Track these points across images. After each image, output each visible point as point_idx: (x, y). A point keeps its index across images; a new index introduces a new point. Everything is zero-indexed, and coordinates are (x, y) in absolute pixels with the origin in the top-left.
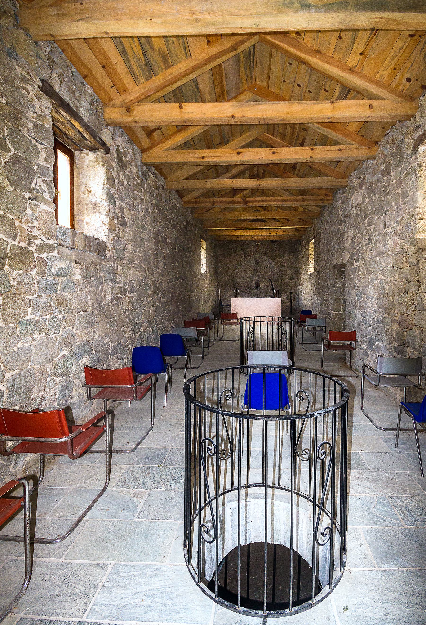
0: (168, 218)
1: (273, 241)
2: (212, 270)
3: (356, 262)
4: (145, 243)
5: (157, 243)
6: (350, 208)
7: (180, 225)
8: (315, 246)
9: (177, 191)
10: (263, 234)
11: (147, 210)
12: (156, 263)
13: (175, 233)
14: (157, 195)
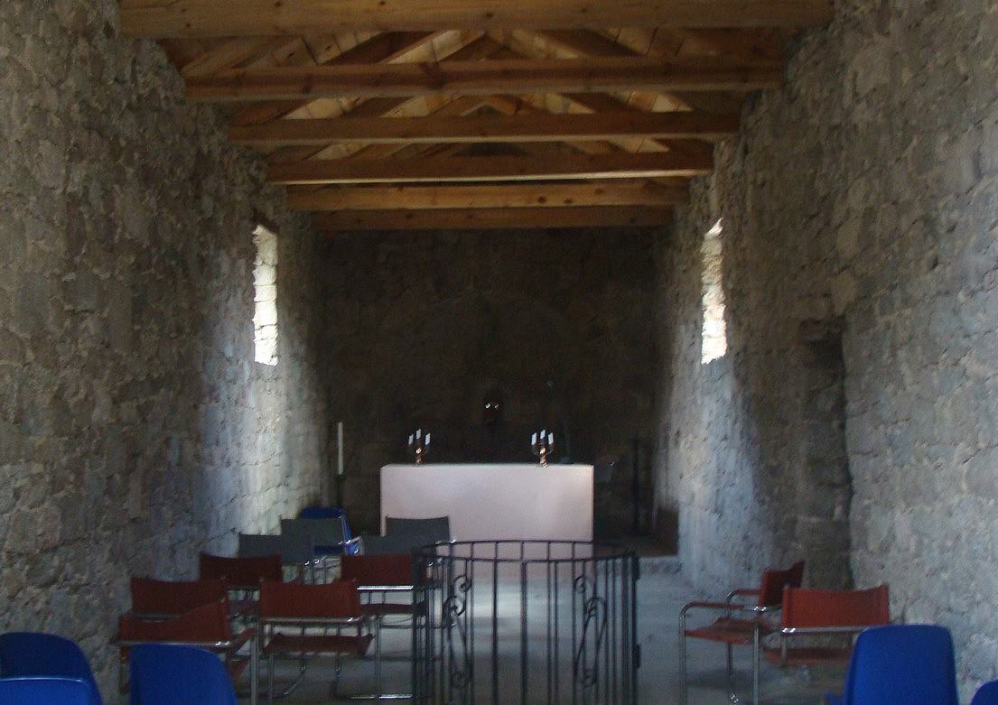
0: (123, 143)
1: (554, 232)
2: (302, 350)
3: (883, 313)
4: (30, 241)
5: (75, 240)
6: (847, 101)
7: (172, 172)
8: (725, 248)
9: (163, 42)
10: (516, 202)
11: (41, 112)
12: (67, 323)
13: (152, 201)
14: (83, 60)
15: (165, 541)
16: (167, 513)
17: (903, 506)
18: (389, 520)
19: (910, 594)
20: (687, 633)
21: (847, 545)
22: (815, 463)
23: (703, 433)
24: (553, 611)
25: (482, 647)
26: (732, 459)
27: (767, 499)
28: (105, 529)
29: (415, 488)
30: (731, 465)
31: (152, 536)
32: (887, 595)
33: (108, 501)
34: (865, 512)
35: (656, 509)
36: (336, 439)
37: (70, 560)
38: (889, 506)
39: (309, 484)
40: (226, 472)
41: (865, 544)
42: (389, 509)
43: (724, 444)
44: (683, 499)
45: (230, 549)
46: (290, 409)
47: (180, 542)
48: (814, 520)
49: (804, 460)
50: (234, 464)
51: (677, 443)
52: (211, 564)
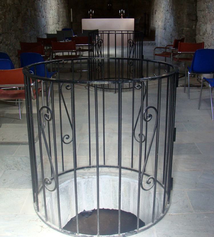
15: (28, 35)
16: (29, 28)
17: (209, 23)
18: (83, 30)
19: (209, 45)
20: (156, 55)
21: (196, 35)
22: (189, 15)
23: (162, 10)
24: (122, 53)
25: (106, 60)
26: (168, 16)
27: (177, 25)
28: (13, 31)
29: (90, 24)
30: (168, 17)
31: (25, 33)
32: (204, 45)
33: (13, 24)
34: (200, 26)
35: (150, 30)
36: (71, 13)
37: (5, 38)
38: (206, 23)
39: (64, 24)
40: (43, 19)
41: (199, 34)
42: (84, 28)
43: (167, 12)
44: (156, 27)
45: (45, 37)
46: (59, 5)
47: (32, 35)
48: (188, 29)
49: (186, 14)
50: (45, 17)
51: (155, 13)
52: (40, 40)
